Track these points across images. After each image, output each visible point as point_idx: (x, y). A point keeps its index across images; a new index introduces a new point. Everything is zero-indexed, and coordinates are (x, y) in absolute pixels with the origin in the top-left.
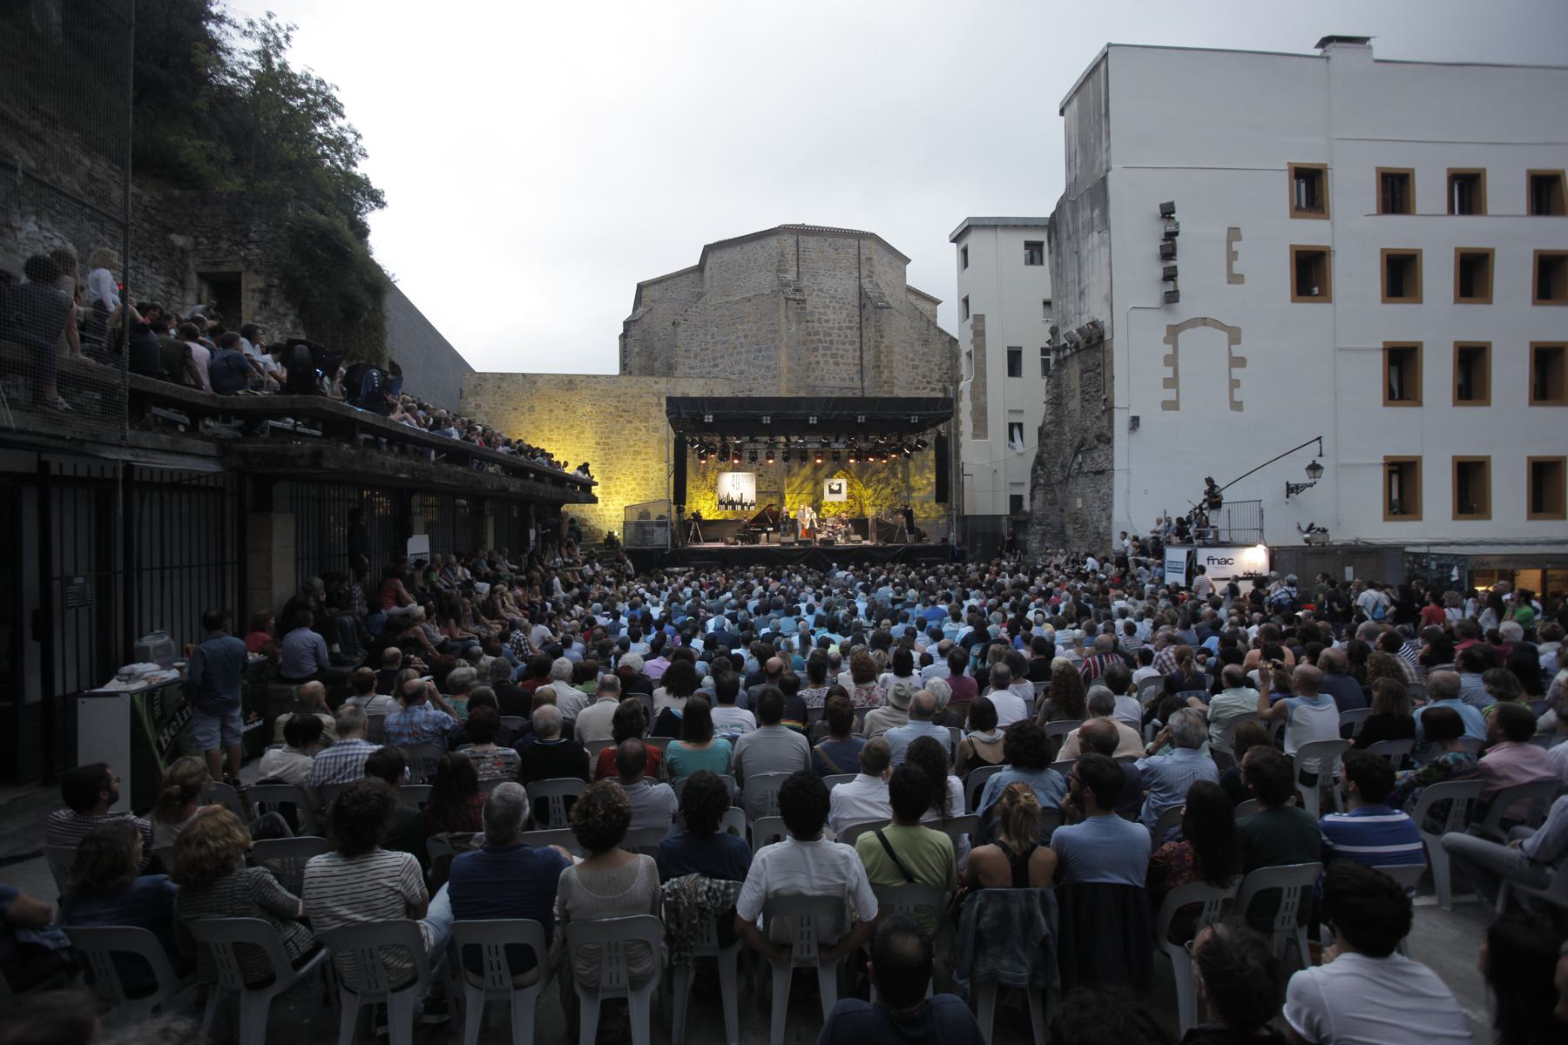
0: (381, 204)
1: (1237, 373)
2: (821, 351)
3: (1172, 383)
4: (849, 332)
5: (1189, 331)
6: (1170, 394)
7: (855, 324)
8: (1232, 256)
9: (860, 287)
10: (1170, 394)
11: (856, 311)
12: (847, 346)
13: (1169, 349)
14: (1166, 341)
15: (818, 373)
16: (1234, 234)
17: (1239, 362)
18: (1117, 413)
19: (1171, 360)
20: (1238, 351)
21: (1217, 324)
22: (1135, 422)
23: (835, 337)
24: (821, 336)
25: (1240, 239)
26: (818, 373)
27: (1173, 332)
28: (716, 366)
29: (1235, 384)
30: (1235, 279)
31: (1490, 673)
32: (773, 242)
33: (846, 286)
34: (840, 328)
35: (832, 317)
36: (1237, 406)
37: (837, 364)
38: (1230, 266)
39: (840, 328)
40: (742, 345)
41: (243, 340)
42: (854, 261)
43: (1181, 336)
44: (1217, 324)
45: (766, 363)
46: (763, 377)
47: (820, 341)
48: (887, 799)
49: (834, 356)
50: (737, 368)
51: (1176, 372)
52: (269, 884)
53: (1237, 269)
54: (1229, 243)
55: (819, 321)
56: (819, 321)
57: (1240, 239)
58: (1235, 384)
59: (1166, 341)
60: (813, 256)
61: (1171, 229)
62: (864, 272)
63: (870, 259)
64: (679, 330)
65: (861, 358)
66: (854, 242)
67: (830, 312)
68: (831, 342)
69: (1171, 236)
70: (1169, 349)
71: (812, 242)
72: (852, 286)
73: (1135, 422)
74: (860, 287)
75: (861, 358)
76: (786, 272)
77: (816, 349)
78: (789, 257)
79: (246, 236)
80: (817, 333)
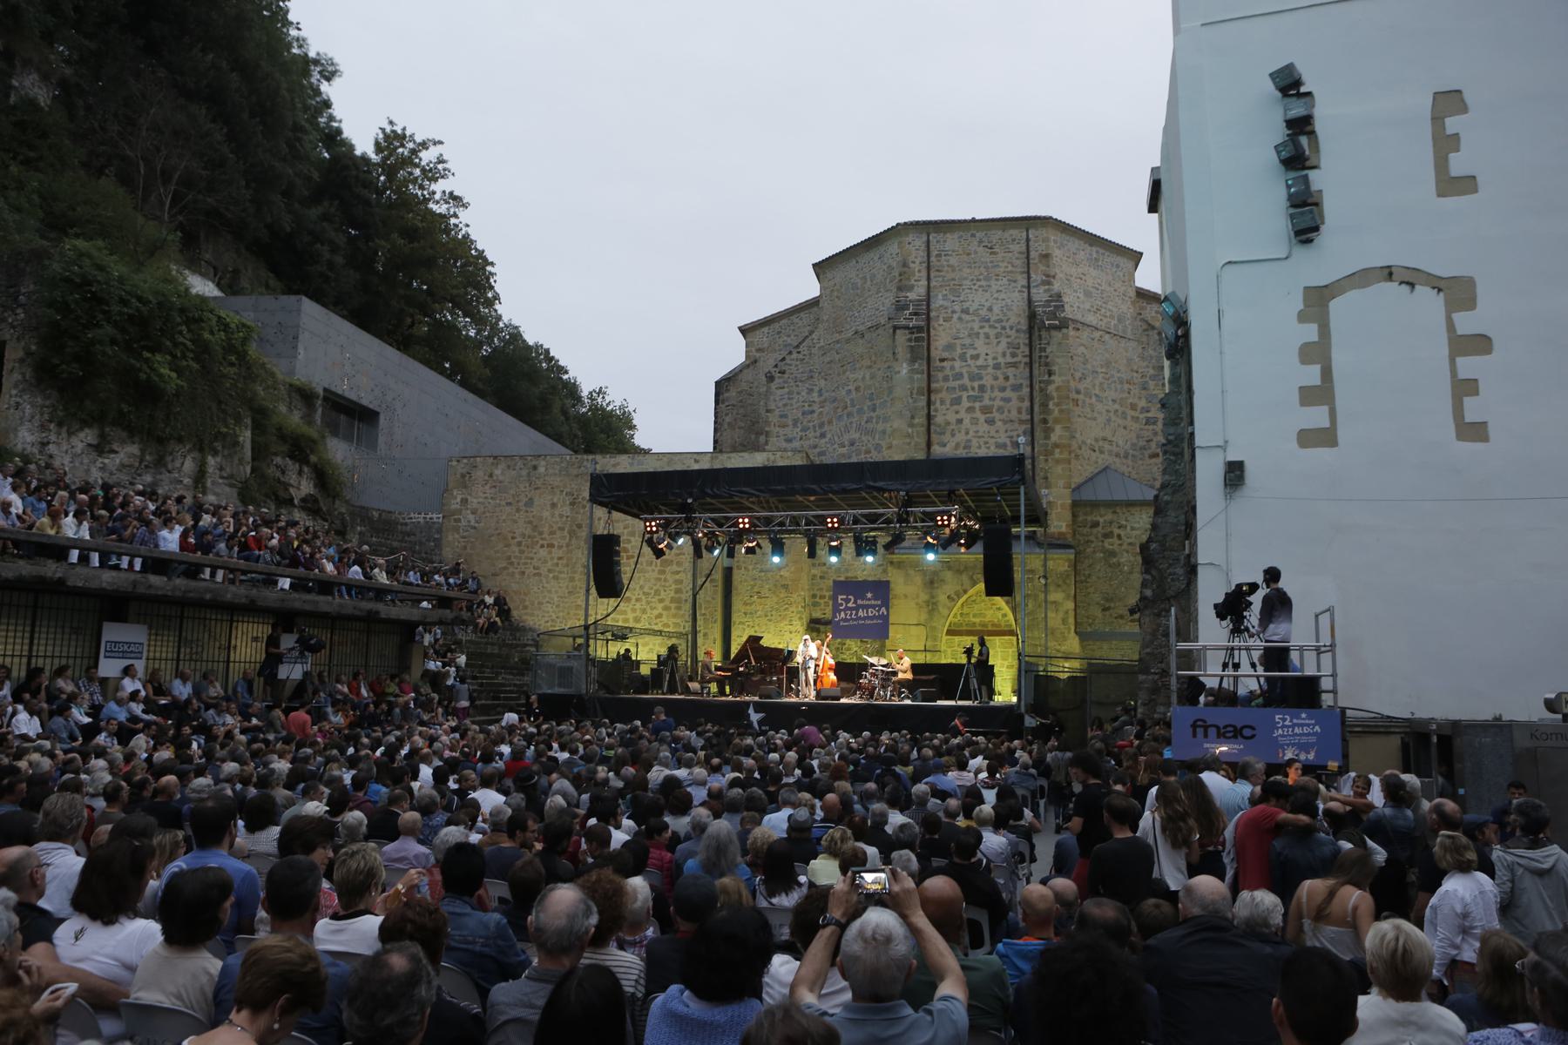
1: (1468, 366)
2: (965, 404)
3: (1320, 394)
4: (1011, 372)
5: (1352, 297)
6: (1317, 417)
7: (1022, 359)
8: (1445, 144)
9: (1030, 301)
10: (1317, 417)
11: (1023, 339)
12: (1008, 393)
13: (1311, 332)
14: (1302, 317)
16: (1449, 102)
17: (1481, 344)
18: (1201, 459)
19: (1317, 353)
20: (1467, 323)
21: (1410, 279)
22: (1235, 474)
23: (988, 381)
24: (966, 381)
25: (1463, 108)
26: (960, 437)
27: (1318, 301)
28: (823, 435)
29: (1464, 388)
30: (1453, 185)
31: (580, 881)
32: (893, 248)
33: (1004, 300)
34: (997, 367)
36: (1474, 432)
37: (990, 422)
38: (1441, 164)
39: (997, 367)
42: (1020, 263)
43: (1336, 306)
44: (1410, 279)
45: (880, 427)
47: (963, 388)
49: (986, 410)
50: (846, 438)
51: (1327, 373)
53: (1458, 165)
54: (1437, 120)
55: (963, 357)
56: (963, 357)
57: (1463, 108)
58: (1464, 388)
59: (1302, 317)
60: (953, 261)
61: (1297, 110)
62: (1036, 277)
63: (1046, 257)
64: (773, 386)
65: (929, 403)
66: (1018, 234)
67: (980, 344)
68: (982, 388)
69: (1301, 126)
70: (1311, 332)
71: (951, 241)
72: (1014, 301)
73: (1235, 474)
74: (1030, 301)
75: (929, 403)
76: (911, 288)
77: (957, 401)
78: (916, 267)
79: (16, 299)
80: (959, 376)
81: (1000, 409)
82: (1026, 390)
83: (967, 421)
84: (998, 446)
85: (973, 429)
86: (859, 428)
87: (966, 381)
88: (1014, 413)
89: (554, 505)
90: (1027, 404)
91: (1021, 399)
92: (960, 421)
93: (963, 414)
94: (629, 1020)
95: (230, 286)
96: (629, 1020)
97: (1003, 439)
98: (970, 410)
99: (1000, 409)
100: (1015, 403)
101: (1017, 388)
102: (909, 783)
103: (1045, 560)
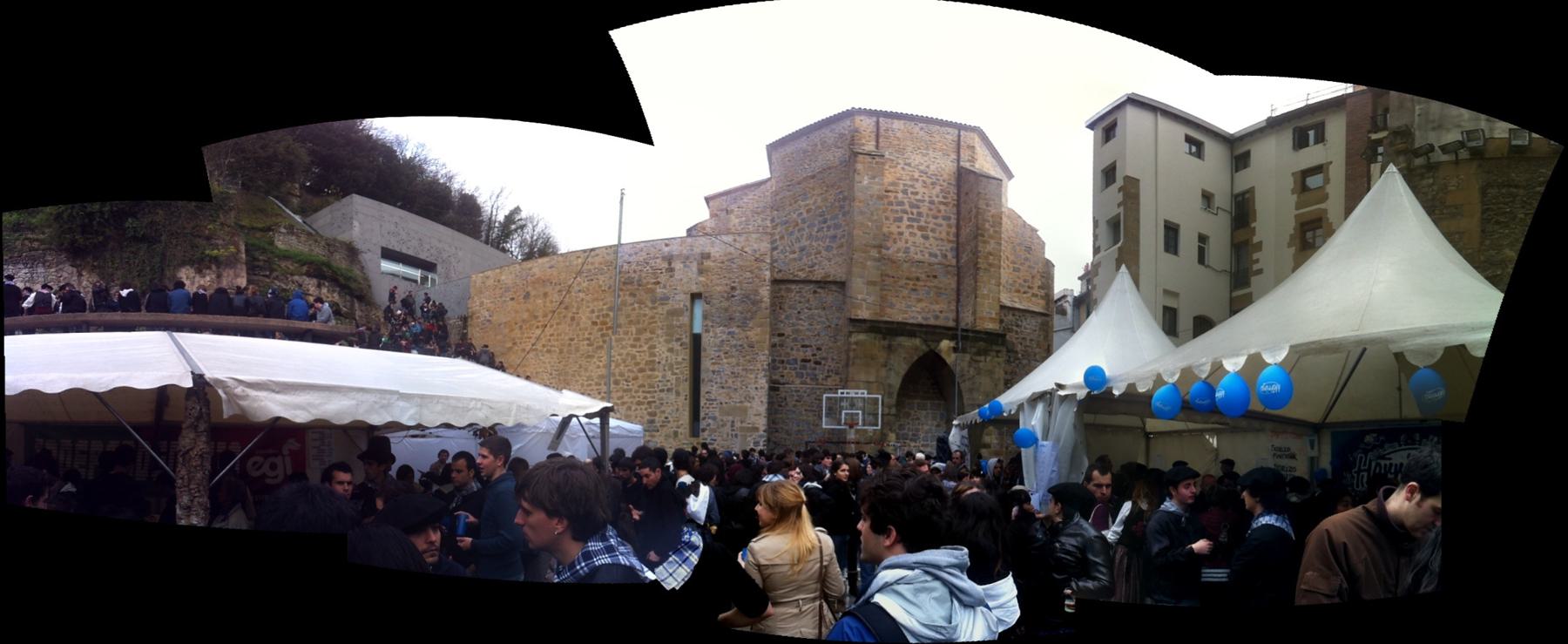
0: (517, 210)
2: (906, 223)
4: (942, 208)
12: (940, 221)
15: (901, 244)
23: (924, 210)
24: (907, 207)
26: (901, 244)
34: (932, 202)
35: (921, 190)
37: (926, 237)
40: (804, 221)
41: (954, 448)
45: (832, 232)
46: (828, 249)
48: (903, 373)
49: (921, 228)
50: (797, 246)
52: (631, 569)
55: (905, 192)
56: (905, 192)
67: (919, 185)
68: (920, 214)
77: (900, 220)
80: (902, 203)
81: (933, 231)
82: (953, 222)
83: (906, 234)
84: (931, 255)
85: (911, 239)
86: (810, 237)
87: (907, 207)
88: (944, 235)
89: (545, 295)
90: (954, 230)
91: (949, 226)
92: (901, 234)
93: (903, 229)
94: (1192, 426)
95: (752, 625)
96: (1192, 426)
97: (935, 250)
98: (909, 227)
99: (933, 231)
100: (945, 228)
101: (945, 218)
102: (460, 530)
103: (957, 320)
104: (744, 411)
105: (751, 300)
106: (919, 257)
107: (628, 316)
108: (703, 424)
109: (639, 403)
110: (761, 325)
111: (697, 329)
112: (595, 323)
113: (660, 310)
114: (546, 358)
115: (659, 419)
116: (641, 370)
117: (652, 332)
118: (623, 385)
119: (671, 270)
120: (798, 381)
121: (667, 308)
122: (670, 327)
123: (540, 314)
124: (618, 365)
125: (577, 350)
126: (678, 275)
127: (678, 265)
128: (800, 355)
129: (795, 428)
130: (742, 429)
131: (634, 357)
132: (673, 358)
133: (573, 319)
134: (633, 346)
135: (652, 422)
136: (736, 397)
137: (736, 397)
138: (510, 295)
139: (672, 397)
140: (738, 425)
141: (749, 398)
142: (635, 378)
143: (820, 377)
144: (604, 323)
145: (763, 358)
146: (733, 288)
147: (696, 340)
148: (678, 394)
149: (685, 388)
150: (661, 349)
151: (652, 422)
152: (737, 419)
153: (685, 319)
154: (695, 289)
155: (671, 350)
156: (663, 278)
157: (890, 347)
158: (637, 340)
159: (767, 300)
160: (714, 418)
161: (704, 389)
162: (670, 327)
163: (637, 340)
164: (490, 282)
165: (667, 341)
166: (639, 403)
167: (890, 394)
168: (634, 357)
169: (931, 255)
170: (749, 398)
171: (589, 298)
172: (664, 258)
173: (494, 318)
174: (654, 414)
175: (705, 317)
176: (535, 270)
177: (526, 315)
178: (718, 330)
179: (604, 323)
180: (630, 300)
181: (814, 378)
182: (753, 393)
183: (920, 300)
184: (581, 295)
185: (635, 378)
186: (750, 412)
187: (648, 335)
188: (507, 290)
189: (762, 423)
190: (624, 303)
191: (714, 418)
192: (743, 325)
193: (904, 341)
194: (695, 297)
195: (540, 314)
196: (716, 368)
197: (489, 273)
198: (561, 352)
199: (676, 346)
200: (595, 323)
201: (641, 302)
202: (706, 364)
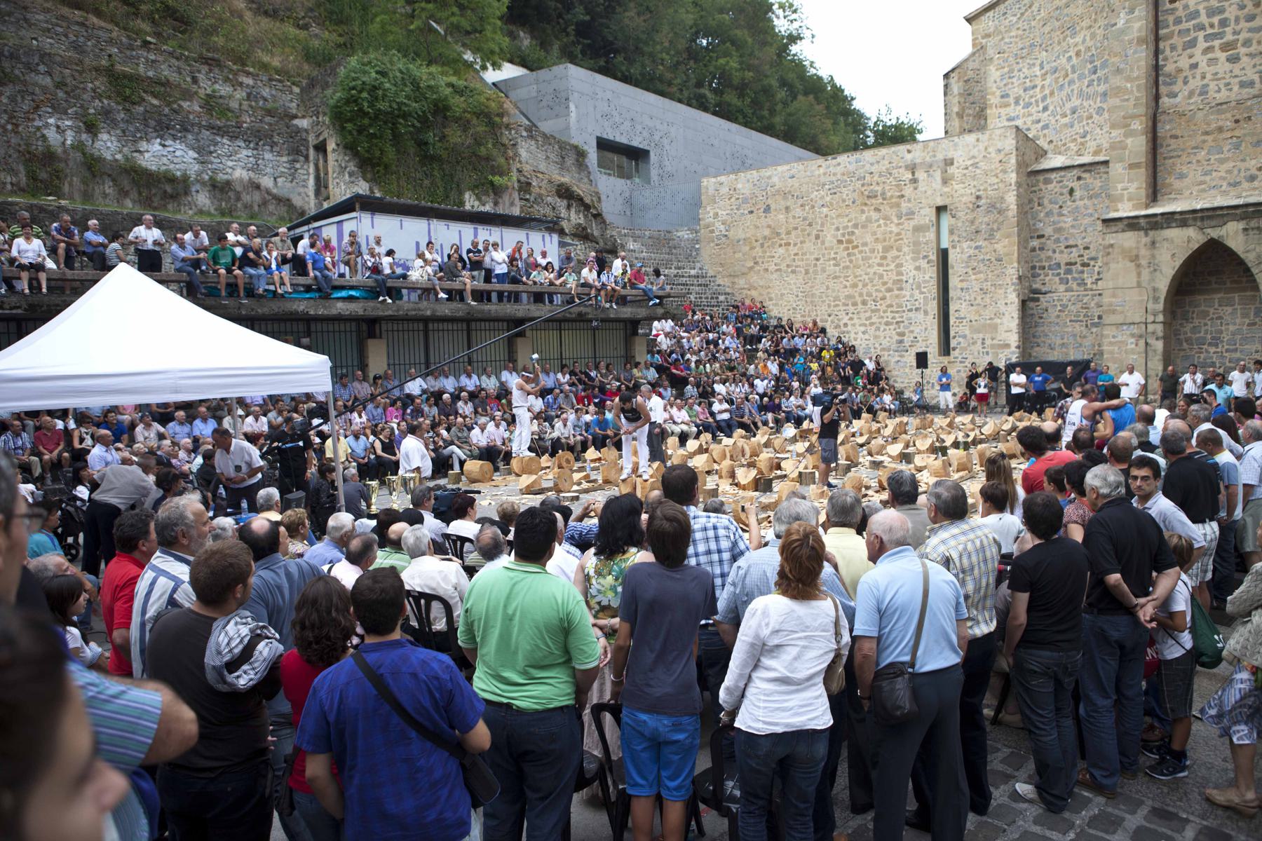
2: (1202, 45)
15: (1195, 83)
24: (1203, 19)
37: (1234, 59)
49: (1226, 47)
83: (1203, 65)
84: (1242, 85)
87: (1203, 19)
92: (1194, 66)
98: (1207, 50)
104: (994, 328)
105: (996, 207)
106: (1223, 95)
107: (874, 233)
108: (953, 343)
109: (887, 324)
110: (1008, 236)
111: (944, 245)
112: (840, 242)
113: (906, 226)
114: (791, 279)
115: (908, 339)
116: (889, 290)
117: (899, 250)
118: (871, 305)
119: (914, 181)
120: (1062, 288)
121: (912, 223)
122: (917, 243)
123: (783, 231)
124: (865, 285)
125: (824, 270)
126: (922, 186)
127: (921, 175)
128: (1062, 258)
129: (1059, 341)
130: (993, 346)
131: (881, 276)
132: (920, 277)
133: (817, 237)
134: (879, 265)
135: (901, 342)
136: (987, 313)
137: (987, 313)
138: (747, 207)
139: (920, 316)
140: (988, 342)
141: (998, 314)
142: (883, 298)
143: (1089, 281)
144: (849, 242)
145: (1012, 271)
146: (978, 197)
147: (944, 255)
148: (926, 313)
149: (933, 307)
150: (909, 267)
151: (901, 342)
152: (988, 336)
153: (931, 235)
154: (940, 203)
155: (918, 268)
156: (908, 191)
157: (1153, 243)
158: (884, 258)
159: (1014, 207)
160: (965, 337)
161: (952, 308)
162: (917, 243)
163: (884, 258)
164: (724, 190)
165: (914, 259)
166: (887, 324)
167: (1156, 300)
168: (881, 276)
169: (1242, 85)
170: (998, 314)
171: (833, 214)
172: (907, 167)
173: (730, 234)
174: (902, 334)
175: (951, 232)
176: (775, 179)
177: (767, 232)
178: (965, 245)
179: (849, 242)
180: (874, 215)
181: (1082, 283)
182: (1003, 309)
183: (1222, 161)
184: (825, 210)
185: (883, 298)
186: (1001, 329)
187: (894, 253)
188: (745, 201)
189: (1014, 339)
190: (869, 220)
191: (965, 337)
192: (990, 237)
193: (1174, 233)
194: (940, 210)
195: (783, 231)
196: (964, 285)
197: (722, 179)
198: (807, 272)
199: (923, 263)
200: (840, 242)
201: (886, 218)
202: (954, 282)
